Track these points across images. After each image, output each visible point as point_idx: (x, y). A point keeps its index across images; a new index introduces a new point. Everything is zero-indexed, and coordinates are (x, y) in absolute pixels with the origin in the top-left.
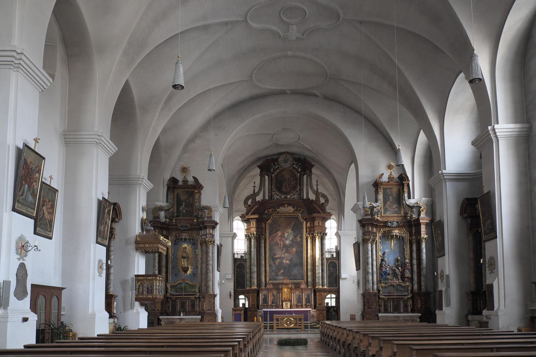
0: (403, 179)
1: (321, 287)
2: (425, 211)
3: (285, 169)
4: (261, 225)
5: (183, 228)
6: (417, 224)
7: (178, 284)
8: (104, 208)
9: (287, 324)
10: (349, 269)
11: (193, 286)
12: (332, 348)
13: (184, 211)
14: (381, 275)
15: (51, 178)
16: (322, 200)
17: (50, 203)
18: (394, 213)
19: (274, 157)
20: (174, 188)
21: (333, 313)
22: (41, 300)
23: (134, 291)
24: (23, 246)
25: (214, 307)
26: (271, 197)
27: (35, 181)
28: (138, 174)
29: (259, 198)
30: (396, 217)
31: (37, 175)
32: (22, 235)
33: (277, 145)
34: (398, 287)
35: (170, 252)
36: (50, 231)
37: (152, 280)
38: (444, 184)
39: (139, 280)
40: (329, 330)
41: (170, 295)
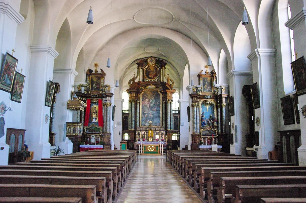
0: (213, 73)
1: (169, 130)
2: (224, 91)
3: (151, 65)
5: (94, 96)
6: (221, 97)
8: (50, 86)
9: (150, 149)
12: (173, 166)
13: (95, 87)
14: (201, 124)
15: (22, 70)
17: (21, 83)
18: (208, 91)
19: (146, 59)
20: (90, 75)
21: (176, 144)
23: (66, 131)
24: (3, 108)
27: (12, 72)
29: (137, 81)
30: (209, 93)
32: (3, 102)
34: (210, 131)
36: (20, 99)
37: (76, 125)
39: (68, 125)
41: (86, 133)
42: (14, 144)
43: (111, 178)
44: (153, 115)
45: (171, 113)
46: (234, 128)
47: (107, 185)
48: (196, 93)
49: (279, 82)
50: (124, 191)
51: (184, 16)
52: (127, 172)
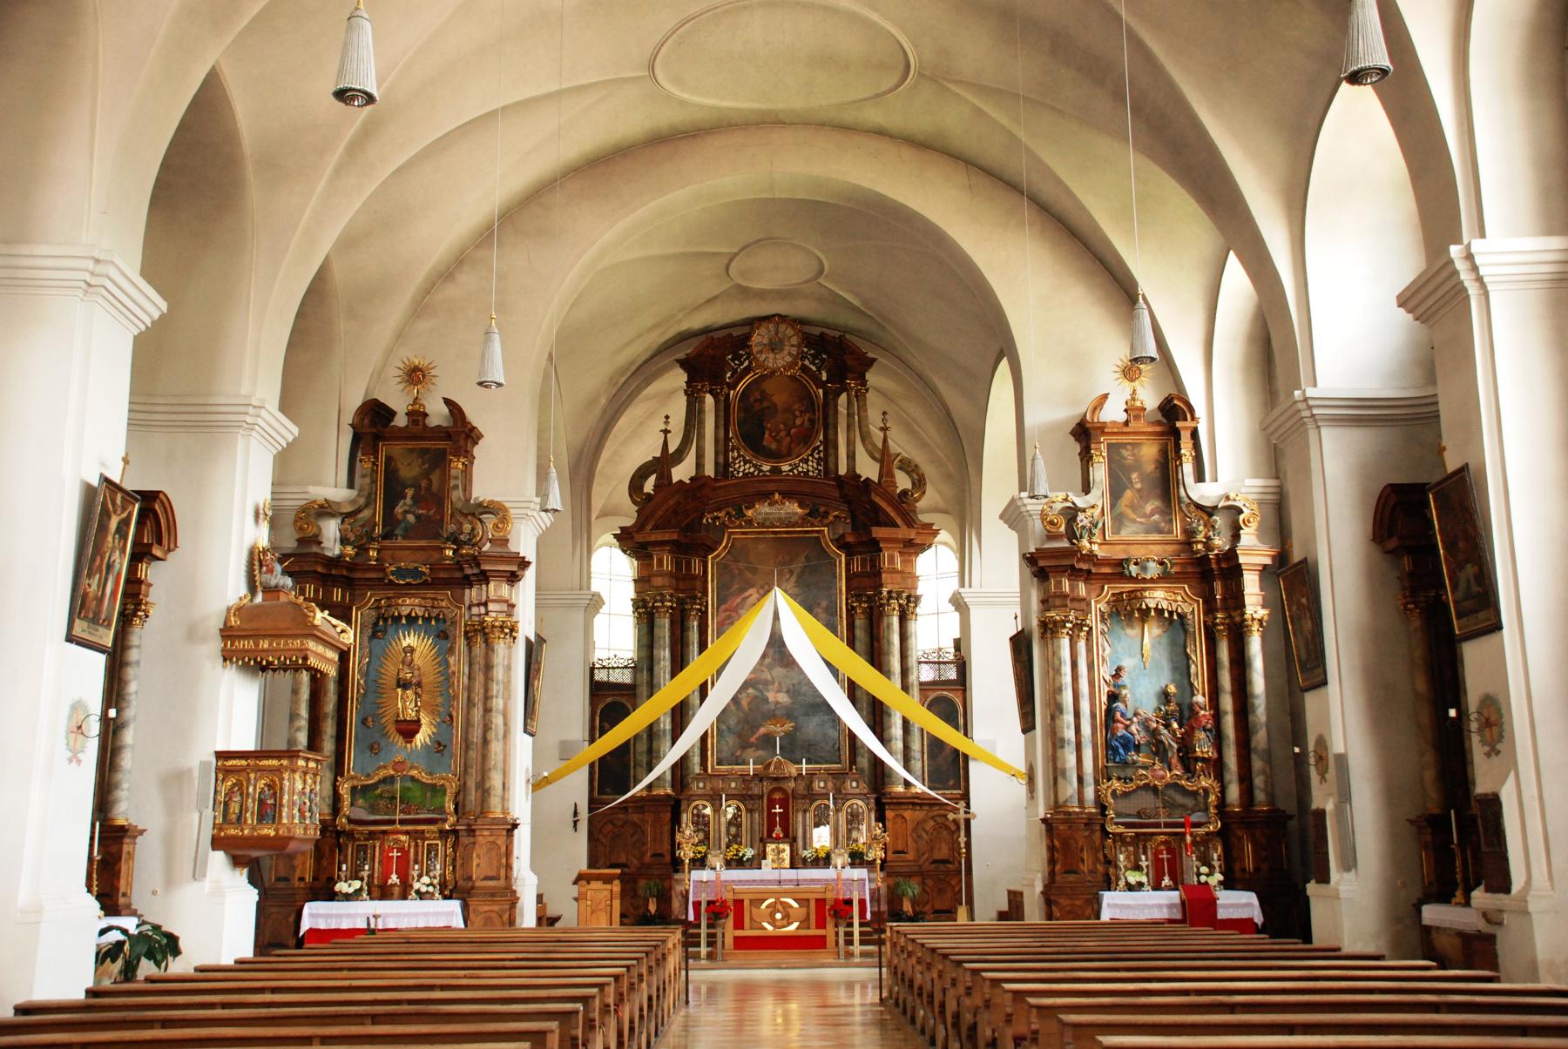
0: (1174, 411)
2: (1254, 526)
3: (773, 372)
4: (689, 564)
5: (404, 577)
6: (1230, 568)
7: (379, 782)
10: (994, 727)
11: (436, 790)
13: (411, 518)
16: (903, 482)
18: (1148, 532)
19: (736, 332)
20: (377, 438)
23: (209, 813)
25: (509, 867)
26: (723, 468)
28: (245, 390)
29: (682, 472)
33: (744, 293)
34: (1171, 792)
35: (354, 664)
37: (278, 771)
38: (1312, 434)
39: (227, 772)
40: (914, 960)
41: (350, 821)
48: (1065, 544)
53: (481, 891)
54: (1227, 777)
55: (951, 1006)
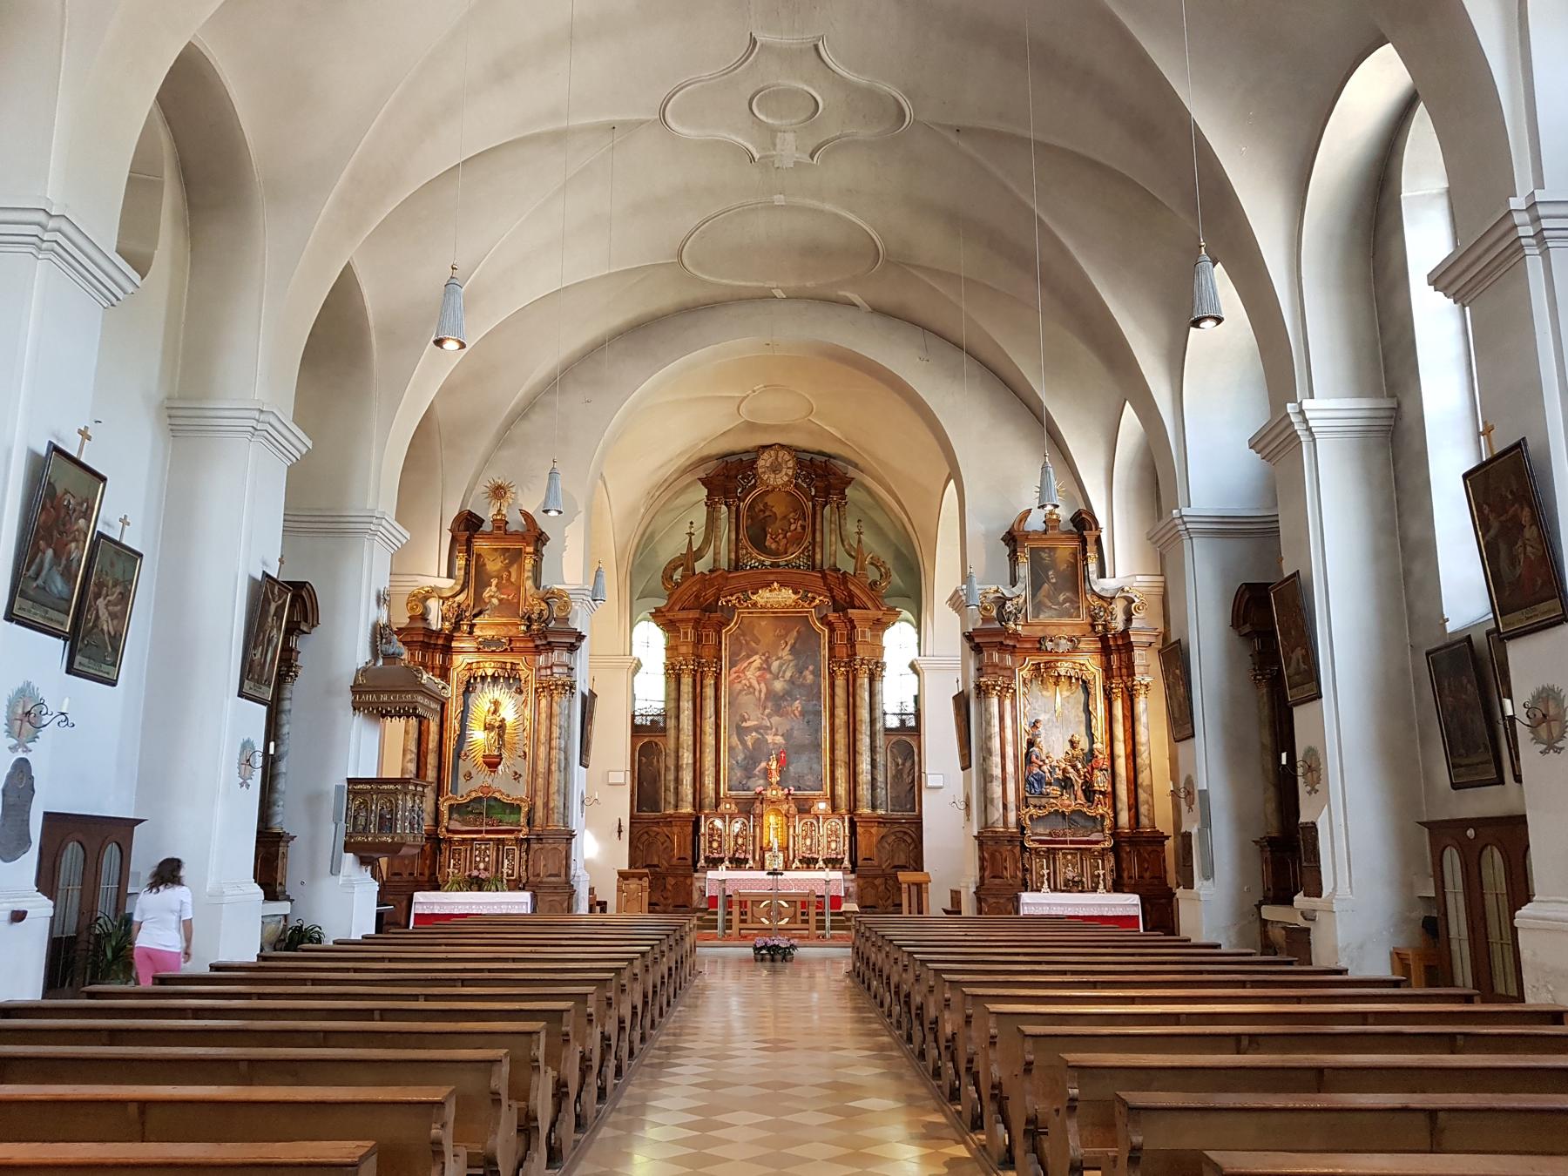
0: (1083, 522)
8: (267, 601)
13: (495, 601)
15: (124, 521)
17: (118, 590)
22: (72, 855)
25: (568, 867)
28: (370, 504)
29: (701, 566)
31: (82, 522)
33: (751, 427)
37: (395, 792)
38: (1187, 543)
41: (448, 831)
42: (77, 894)
43: (541, 1054)
44: (787, 736)
45: (879, 726)
46: (1196, 806)
47: (520, 1091)
48: (997, 625)
49: (1417, 567)
50: (616, 1126)
51: (931, 243)
52: (638, 1028)
53: (553, 888)
54: (1119, 806)
55: (894, 979)
